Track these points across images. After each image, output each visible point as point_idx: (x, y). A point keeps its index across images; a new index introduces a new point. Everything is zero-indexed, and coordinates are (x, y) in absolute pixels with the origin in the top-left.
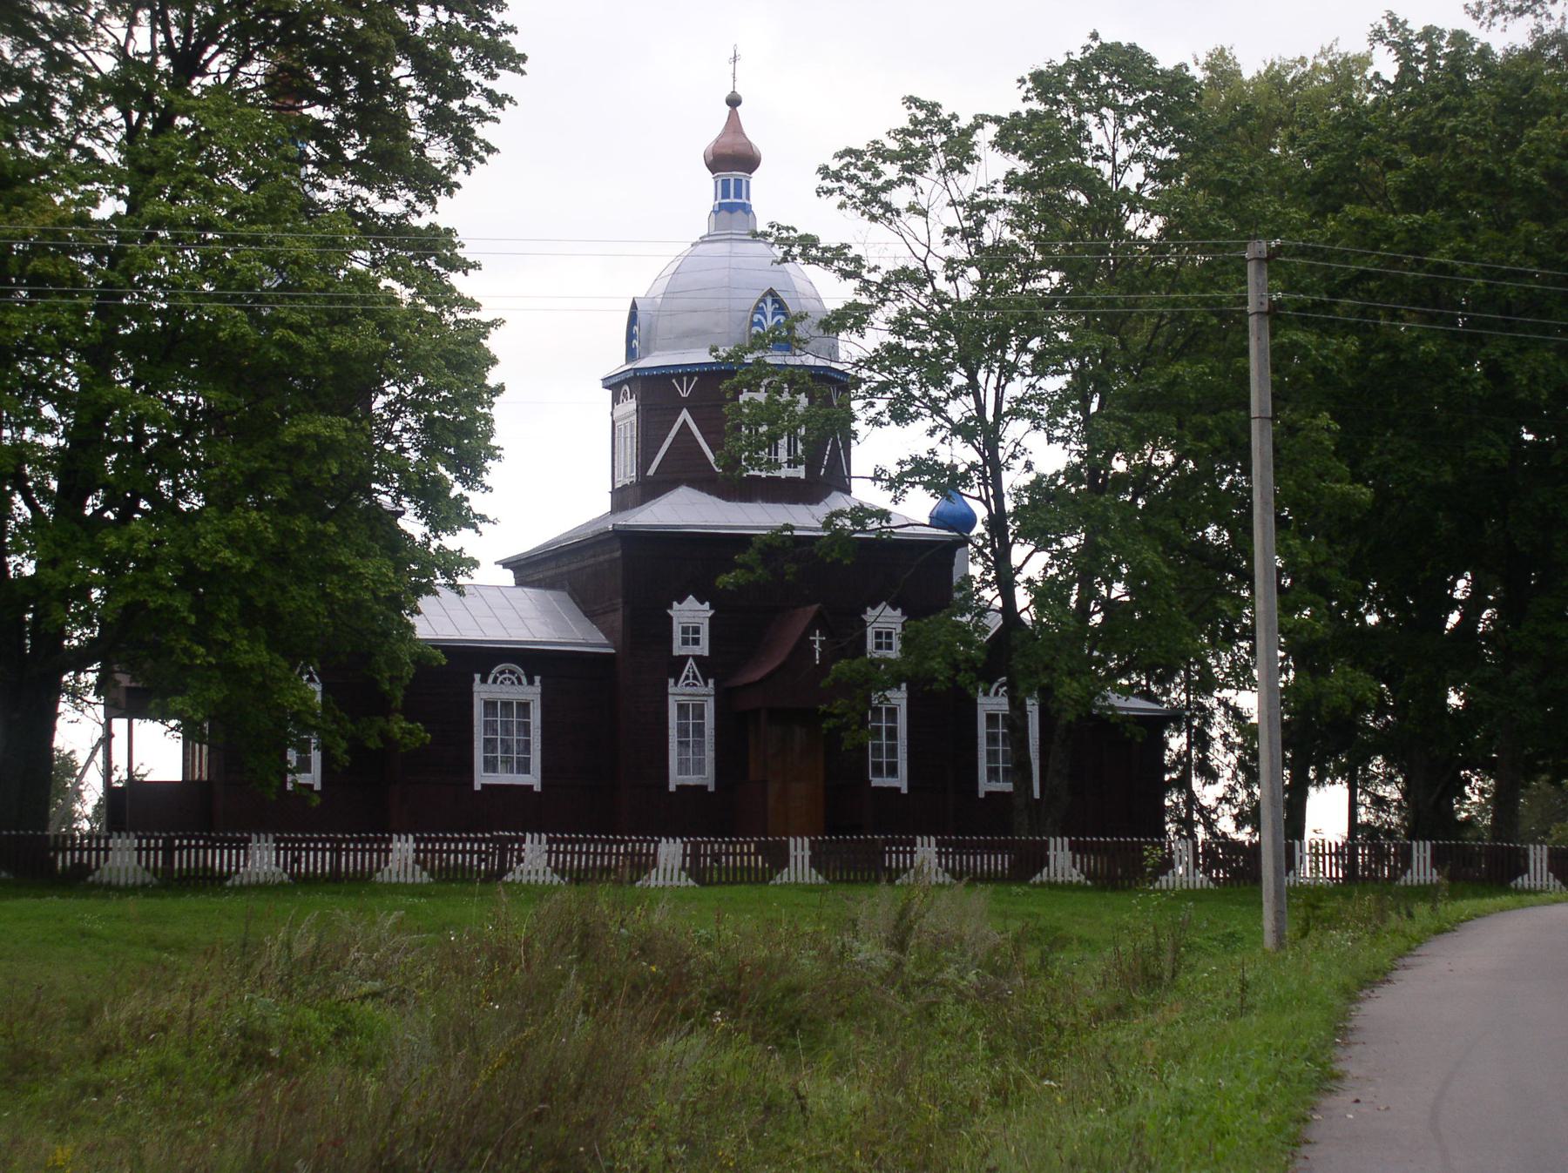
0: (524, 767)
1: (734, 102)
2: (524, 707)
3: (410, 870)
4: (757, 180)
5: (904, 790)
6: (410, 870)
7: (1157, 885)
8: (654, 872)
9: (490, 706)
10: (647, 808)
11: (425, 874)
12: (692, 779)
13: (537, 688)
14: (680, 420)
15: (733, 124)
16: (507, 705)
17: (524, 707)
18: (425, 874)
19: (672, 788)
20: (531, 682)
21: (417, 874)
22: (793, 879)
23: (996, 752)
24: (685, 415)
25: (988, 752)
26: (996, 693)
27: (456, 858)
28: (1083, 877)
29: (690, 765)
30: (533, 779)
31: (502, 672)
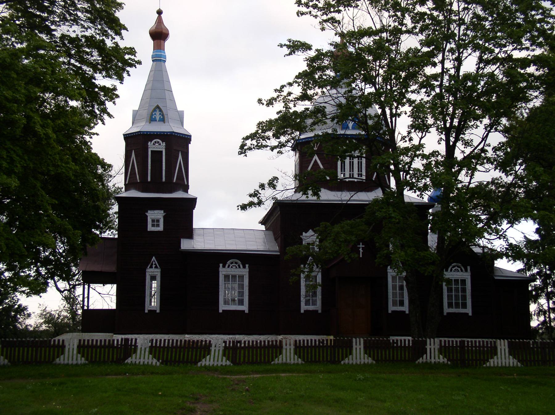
0: (241, 302)
1: (160, 12)
2: (464, 282)
3: (75, 357)
4: (168, 44)
5: (470, 314)
6: (75, 357)
7: (488, 364)
8: (208, 357)
9: (227, 277)
10: (289, 319)
11: (83, 359)
12: (311, 308)
13: (247, 269)
14: (314, 159)
15: (159, 21)
16: (456, 281)
17: (464, 282)
18: (83, 359)
19: (302, 311)
20: (244, 267)
21: (79, 359)
22: (284, 361)
23: (452, 296)
24: (316, 157)
25: (448, 296)
26: (451, 270)
27: (476, 356)
28: (446, 360)
29: (310, 303)
30: (245, 308)
31: (232, 263)
